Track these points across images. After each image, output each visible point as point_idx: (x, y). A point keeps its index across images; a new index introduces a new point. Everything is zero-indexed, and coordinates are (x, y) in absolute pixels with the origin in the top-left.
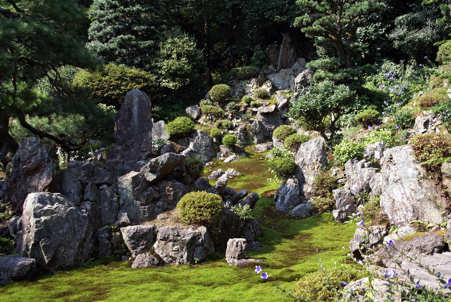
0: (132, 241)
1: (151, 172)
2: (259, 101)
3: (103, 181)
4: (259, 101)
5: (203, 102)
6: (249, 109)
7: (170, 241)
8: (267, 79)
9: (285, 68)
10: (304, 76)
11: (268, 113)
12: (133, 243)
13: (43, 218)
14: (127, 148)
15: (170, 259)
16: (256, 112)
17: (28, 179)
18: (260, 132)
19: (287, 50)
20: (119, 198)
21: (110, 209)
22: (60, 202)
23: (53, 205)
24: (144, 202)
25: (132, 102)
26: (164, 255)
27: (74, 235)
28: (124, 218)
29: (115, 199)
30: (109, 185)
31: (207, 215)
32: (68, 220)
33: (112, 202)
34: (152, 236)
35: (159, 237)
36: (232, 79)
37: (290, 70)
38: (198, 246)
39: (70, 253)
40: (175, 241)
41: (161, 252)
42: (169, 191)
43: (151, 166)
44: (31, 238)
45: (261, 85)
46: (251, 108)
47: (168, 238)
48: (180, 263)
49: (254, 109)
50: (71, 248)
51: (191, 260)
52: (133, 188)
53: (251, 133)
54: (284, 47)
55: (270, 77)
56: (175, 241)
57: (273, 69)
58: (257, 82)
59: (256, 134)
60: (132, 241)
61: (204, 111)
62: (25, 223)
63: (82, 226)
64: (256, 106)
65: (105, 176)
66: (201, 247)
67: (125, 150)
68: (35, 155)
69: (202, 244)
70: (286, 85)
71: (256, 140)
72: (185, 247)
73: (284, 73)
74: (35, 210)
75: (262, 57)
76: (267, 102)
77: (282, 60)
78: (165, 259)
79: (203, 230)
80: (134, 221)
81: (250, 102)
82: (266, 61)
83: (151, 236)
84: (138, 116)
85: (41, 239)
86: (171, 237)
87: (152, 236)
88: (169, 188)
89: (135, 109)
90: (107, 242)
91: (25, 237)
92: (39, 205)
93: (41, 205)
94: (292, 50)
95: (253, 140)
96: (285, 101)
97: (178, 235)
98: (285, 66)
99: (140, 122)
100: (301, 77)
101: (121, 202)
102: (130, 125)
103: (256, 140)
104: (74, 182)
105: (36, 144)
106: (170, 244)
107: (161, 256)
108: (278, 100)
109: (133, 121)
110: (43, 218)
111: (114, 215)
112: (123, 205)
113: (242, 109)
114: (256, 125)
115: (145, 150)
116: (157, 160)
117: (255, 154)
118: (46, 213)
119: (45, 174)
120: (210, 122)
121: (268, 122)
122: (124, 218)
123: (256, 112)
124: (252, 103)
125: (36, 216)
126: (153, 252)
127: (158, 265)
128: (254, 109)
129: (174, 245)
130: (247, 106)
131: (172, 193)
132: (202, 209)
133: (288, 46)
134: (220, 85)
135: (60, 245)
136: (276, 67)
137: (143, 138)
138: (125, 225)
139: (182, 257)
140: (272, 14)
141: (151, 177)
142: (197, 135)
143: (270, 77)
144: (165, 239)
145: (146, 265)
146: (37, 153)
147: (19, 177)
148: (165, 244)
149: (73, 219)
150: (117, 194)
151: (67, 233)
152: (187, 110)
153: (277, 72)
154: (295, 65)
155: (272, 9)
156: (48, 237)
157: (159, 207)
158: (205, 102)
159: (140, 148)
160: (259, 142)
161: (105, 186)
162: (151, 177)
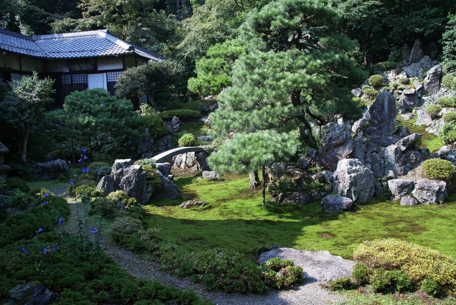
0: (400, 189)
1: (403, 145)
2: (402, 86)
3: (374, 150)
4: (402, 86)
5: (364, 86)
6: (396, 91)
7: (425, 190)
8: (402, 70)
9: (415, 63)
10: (436, 69)
11: (411, 94)
12: (400, 190)
13: (353, 175)
14: (380, 129)
15: (423, 201)
16: (401, 93)
17: (336, 149)
18: (403, 106)
19: (417, 50)
20: (384, 162)
21: (380, 168)
22: (360, 165)
23: (356, 166)
24: (401, 164)
25: (384, 99)
26: (420, 198)
27: (368, 184)
28: (391, 173)
29: (382, 162)
30: (377, 152)
31: (447, 174)
32: (365, 176)
33: (381, 164)
34: (411, 186)
35: (417, 186)
36: (376, 70)
37: (418, 64)
38: (441, 193)
39: (365, 195)
40: (428, 190)
41: (418, 196)
42: (412, 157)
43: (404, 142)
44: (346, 186)
45: (398, 74)
46: (397, 91)
47: (424, 188)
48: (430, 203)
49: (400, 91)
50: (366, 192)
51: (437, 202)
52: (395, 156)
53: (398, 107)
54: (415, 49)
55: (404, 68)
56: (428, 190)
57: (406, 63)
58: (396, 72)
59: (401, 108)
60: (400, 189)
61: (364, 91)
62: (340, 177)
63: (371, 179)
64: (402, 89)
65: (374, 147)
66: (443, 194)
67: (379, 129)
68: (342, 135)
69: (444, 193)
70: (415, 73)
71: (400, 112)
72: (435, 194)
73: (414, 66)
74: (348, 169)
75: (397, 55)
76: (408, 86)
77: (413, 58)
78: (420, 200)
79: (443, 183)
80: (396, 176)
81: (397, 87)
82: (399, 59)
83: (411, 186)
84: (388, 109)
85: (352, 187)
86: (426, 188)
87: (411, 186)
88: (413, 156)
89: (386, 103)
90: (381, 188)
91: (341, 185)
92: (350, 166)
93: (351, 167)
94: (421, 50)
95: (399, 111)
96: (421, 86)
97: (430, 187)
98: (415, 61)
99: (389, 112)
100: (434, 70)
101: (386, 164)
102: (383, 114)
103: (400, 112)
104: (361, 151)
105: (343, 129)
106: (425, 192)
107: (418, 198)
108: (415, 85)
109: (384, 112)
110: (353, 175)
111: (383, 172)
112: (387, 166)
113: (391, 91)
114: (401, 102)
115: (392, 130)
116: (408, 138)
117: (403, 121)
118: (354, 171)
119: (347, 147)
120: (368, 99)
121: (409, 100)
122: (391, 173)
123: (401, 93)
124: (398, 87)
125: (349, 173)
126: (412, 196)
127: (418, 204)
128: (400, 91)
129: (427, 193)
130: (394, 89)
131: (414, 158)
132: (443, 170)
133: (418, 48)
134: (377, 75)
135: (361, 191)
136: (408, 62)
137: (390, 122)
138: (391, 178)
139: (432, 200)
140: (412, 27)
141: (403, 148)
142: (367, 109)
143: (404, 68)
144: (422, 189)
145: (411, 204)
146: (343, 134)
147: (331, 148)
148: (421, 192)
149: (367, 175)
150: (383, 159)
151: (365, 183)
152: (352, 91)
153: (409, 65)
154: (422, 60)
155: (412, 24)
156: (356, 186)
157: (408, 167)
158: (366, 86)
159: (388, 128)
160: (402, 113)
161: (375, 153)
162: (403, 148)
